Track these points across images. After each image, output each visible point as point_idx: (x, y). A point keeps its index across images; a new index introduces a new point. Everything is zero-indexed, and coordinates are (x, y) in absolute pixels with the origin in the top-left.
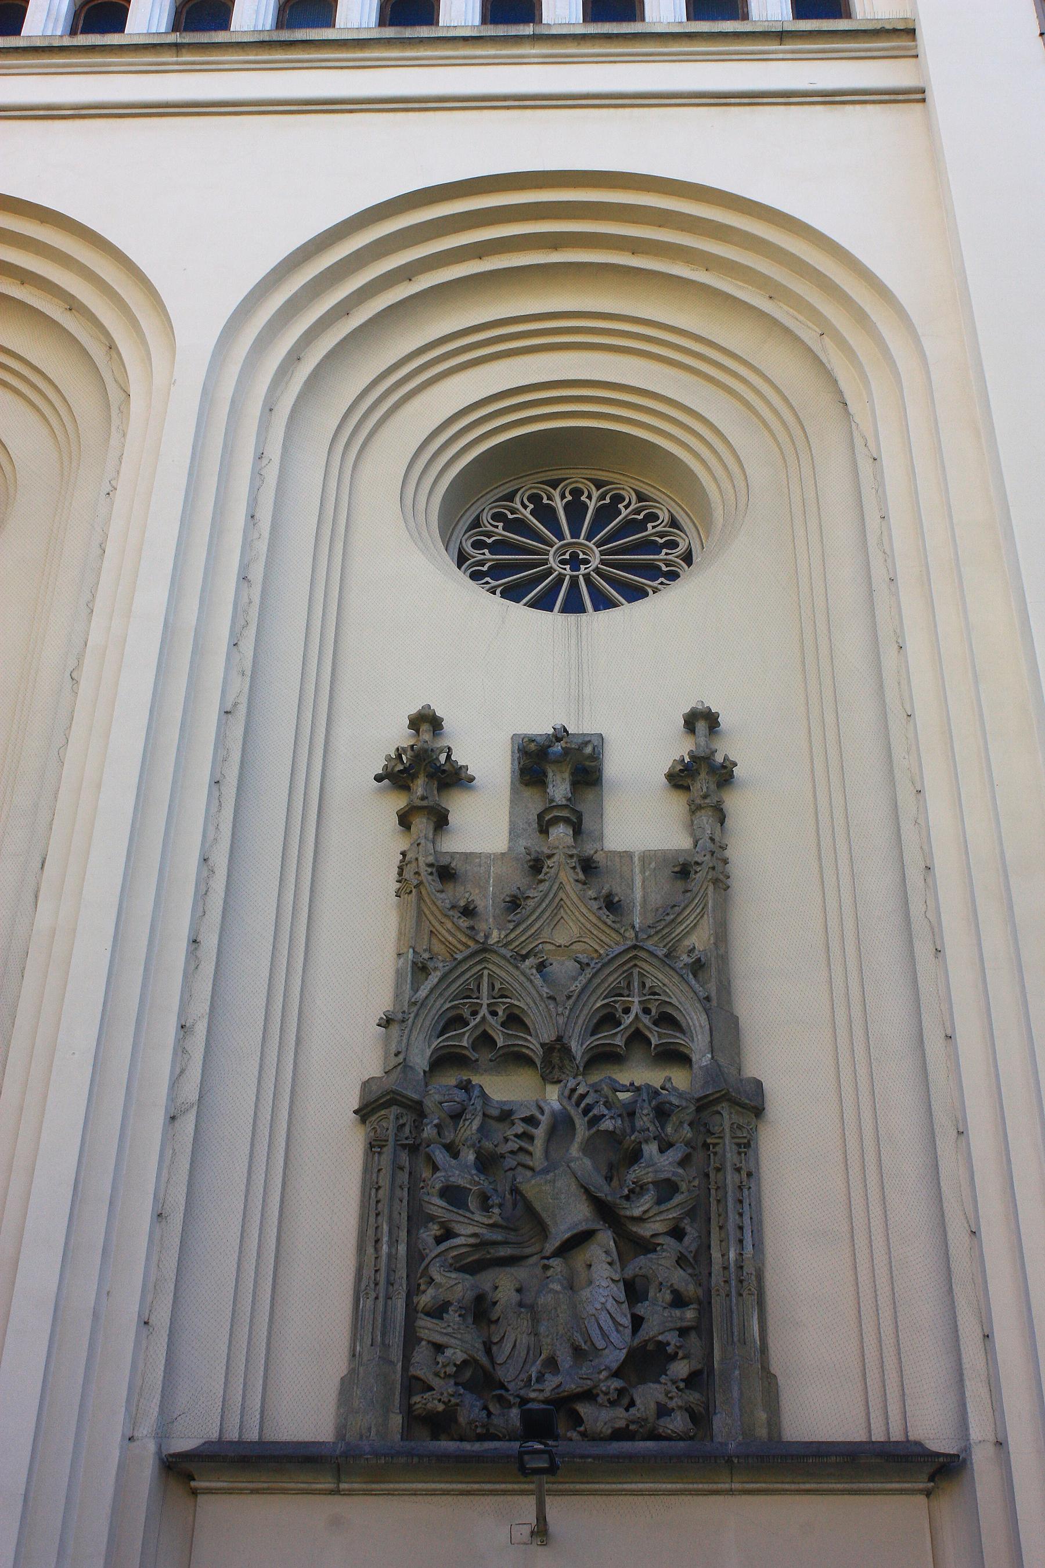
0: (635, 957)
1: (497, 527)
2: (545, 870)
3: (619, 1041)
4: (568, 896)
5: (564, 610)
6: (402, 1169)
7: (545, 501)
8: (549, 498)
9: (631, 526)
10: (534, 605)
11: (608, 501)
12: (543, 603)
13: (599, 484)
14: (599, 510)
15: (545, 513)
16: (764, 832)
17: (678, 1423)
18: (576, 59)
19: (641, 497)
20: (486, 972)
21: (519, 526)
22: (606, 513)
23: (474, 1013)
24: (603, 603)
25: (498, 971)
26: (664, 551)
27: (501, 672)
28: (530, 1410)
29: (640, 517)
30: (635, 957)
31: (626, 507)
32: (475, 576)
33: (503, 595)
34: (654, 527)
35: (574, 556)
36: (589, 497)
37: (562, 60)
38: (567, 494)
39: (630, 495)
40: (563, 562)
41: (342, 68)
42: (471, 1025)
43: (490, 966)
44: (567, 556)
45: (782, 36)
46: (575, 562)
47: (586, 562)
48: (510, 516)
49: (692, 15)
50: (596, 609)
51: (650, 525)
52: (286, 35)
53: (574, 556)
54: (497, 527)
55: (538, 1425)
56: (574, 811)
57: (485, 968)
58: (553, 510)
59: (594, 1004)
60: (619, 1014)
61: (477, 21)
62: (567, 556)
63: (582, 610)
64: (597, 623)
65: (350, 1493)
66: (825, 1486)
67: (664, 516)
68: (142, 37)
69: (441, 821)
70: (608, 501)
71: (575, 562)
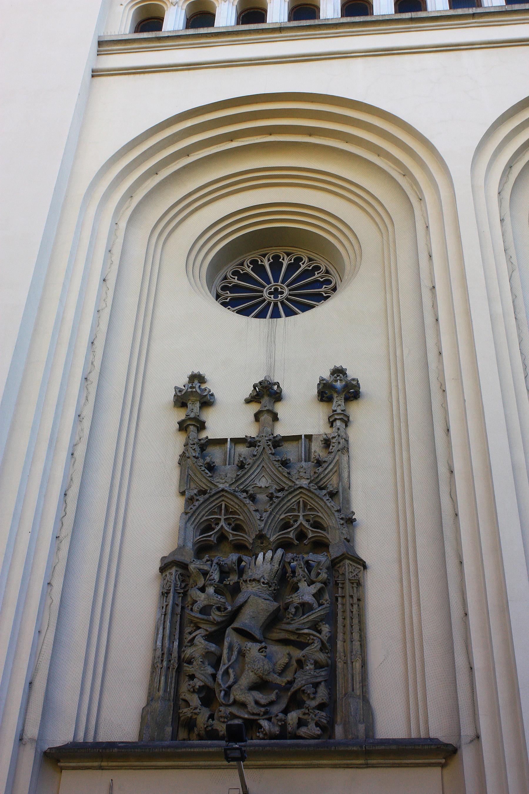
0: (301, 492)
1: (235, 279)
2: (331, 447)
3: (213, 539)
4: (266, 464)
5: (272, 317)
6: (177, 605)
7: (260, 263)
8: (262, 262)
9: (307, 273)
10: (257, 316)
11: (292, 261)
12: (261, 315)
13: (288, 254)
14: (289, 265)
15: (259, 269)
16: (368, 427)
17: (313, 729)
18: (425, 29)
19: (310, 260)
20: (223, 503)
21: (245, 277)
22: (293, 267)
23: (296, 521)
24: (290, 313)
25: (229, 501)
26: (324, 286)
27: (232, 351)
28: (230, 725)
29: (310, 268)
30: (223, 495)
31: (303, 264)
32: (225, 304)
33: (237, 313)
34: (318, 273)
35: (276, 290)
36: (283, 259)
37: (419, 29)
38: (271, 259)
39: (305, 259)
40: (270, 293)
41: (276, 41)
42: (215, 531)
43: (226, 499)
44: (272, 290)
45: (280, 29)
46: (276, 293)
47: (282, 293)
48: (242, 272)
49: (292, 18)
50: (287, 315)
51: (316, 273)
52: (509, 8)
53: (276, 290)
54: (235, 279)
55: (235, 734)
56: (346, 415)
57: (223, 500)
58: (263, 267)
59: (201, 519)
60: (213, 526)
61: (286, 19)
62: (272, 290)
63: (280, 317)
64: (284, 322)
65: (373, 766)
66: (145, 764)
67: (323, 268)
68: (500, 8)
69: (201, 426)
70: (292, 261)
71: (276, 293)
